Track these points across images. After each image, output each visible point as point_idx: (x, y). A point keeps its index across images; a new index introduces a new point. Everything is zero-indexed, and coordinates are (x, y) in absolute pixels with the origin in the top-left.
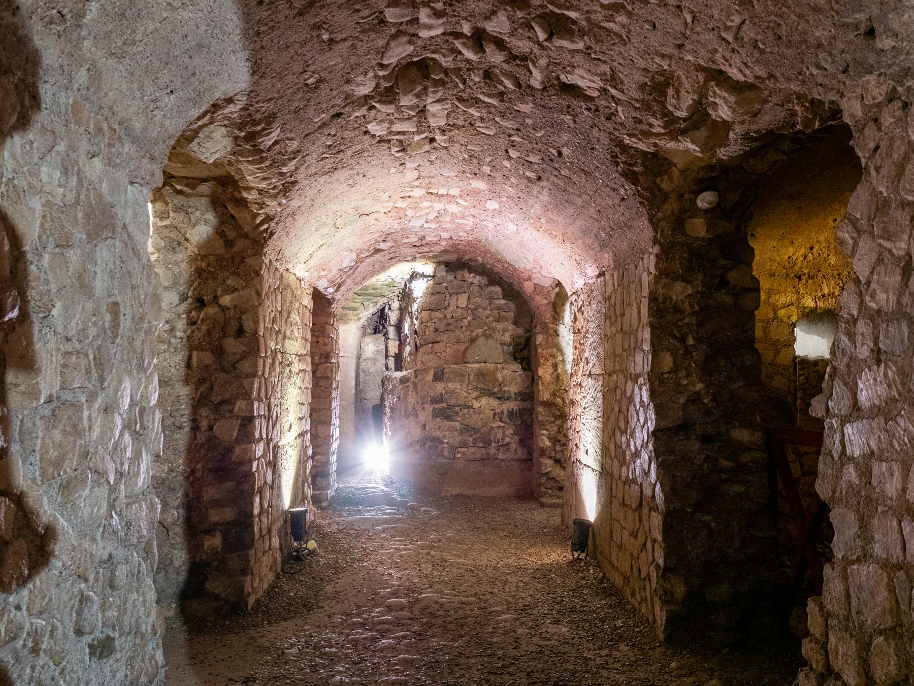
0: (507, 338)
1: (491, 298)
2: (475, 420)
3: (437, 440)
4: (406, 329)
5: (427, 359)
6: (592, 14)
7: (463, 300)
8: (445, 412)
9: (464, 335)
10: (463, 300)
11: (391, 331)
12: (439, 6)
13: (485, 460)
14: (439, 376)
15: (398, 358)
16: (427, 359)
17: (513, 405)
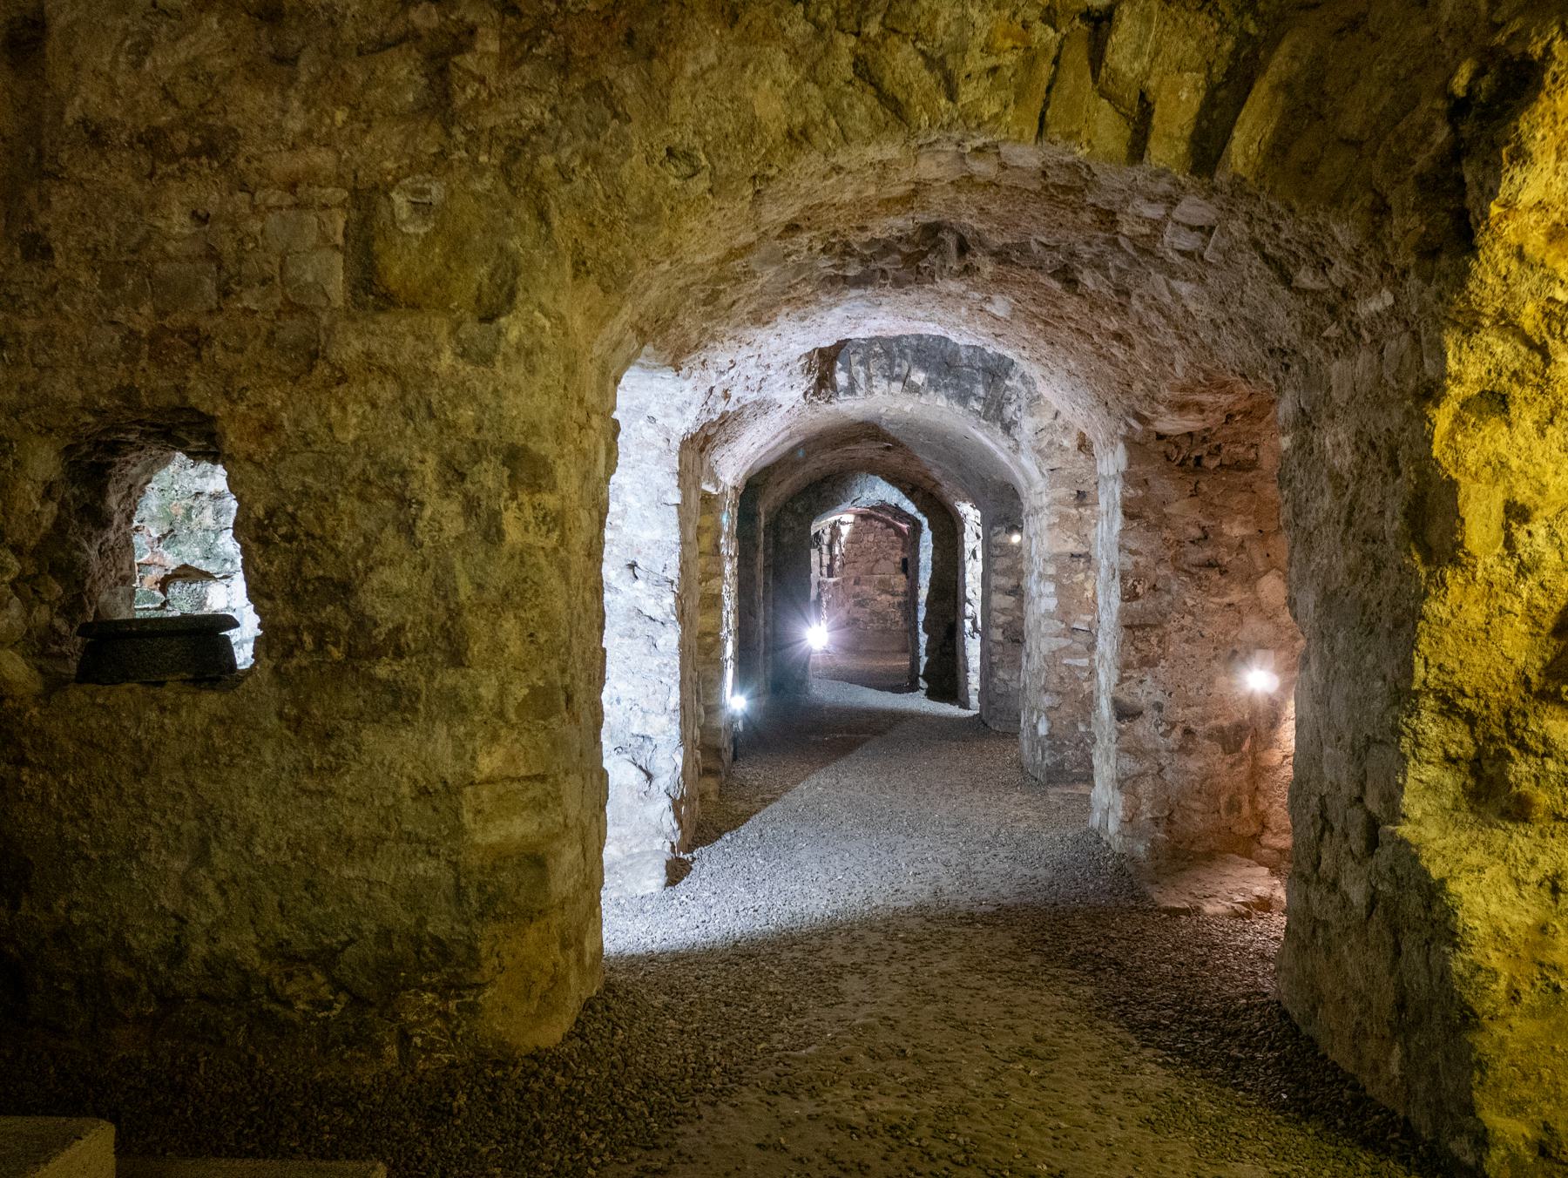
0: (898, 559)
1: (888, 536)
2: (878, 608)
3: (856, 620)
4: (837, 550)
5: (851, 572)
6: (1544, 853)
7: (871, 538)
8: (861, 604)
9: (872, 558)
10: (871, 538)
11: (825, 549)
12: (9, 463)
13: (884, 631)
14: (857, 583)
15: (830, 567)
16: (851, 572)
17: (900, 599)
